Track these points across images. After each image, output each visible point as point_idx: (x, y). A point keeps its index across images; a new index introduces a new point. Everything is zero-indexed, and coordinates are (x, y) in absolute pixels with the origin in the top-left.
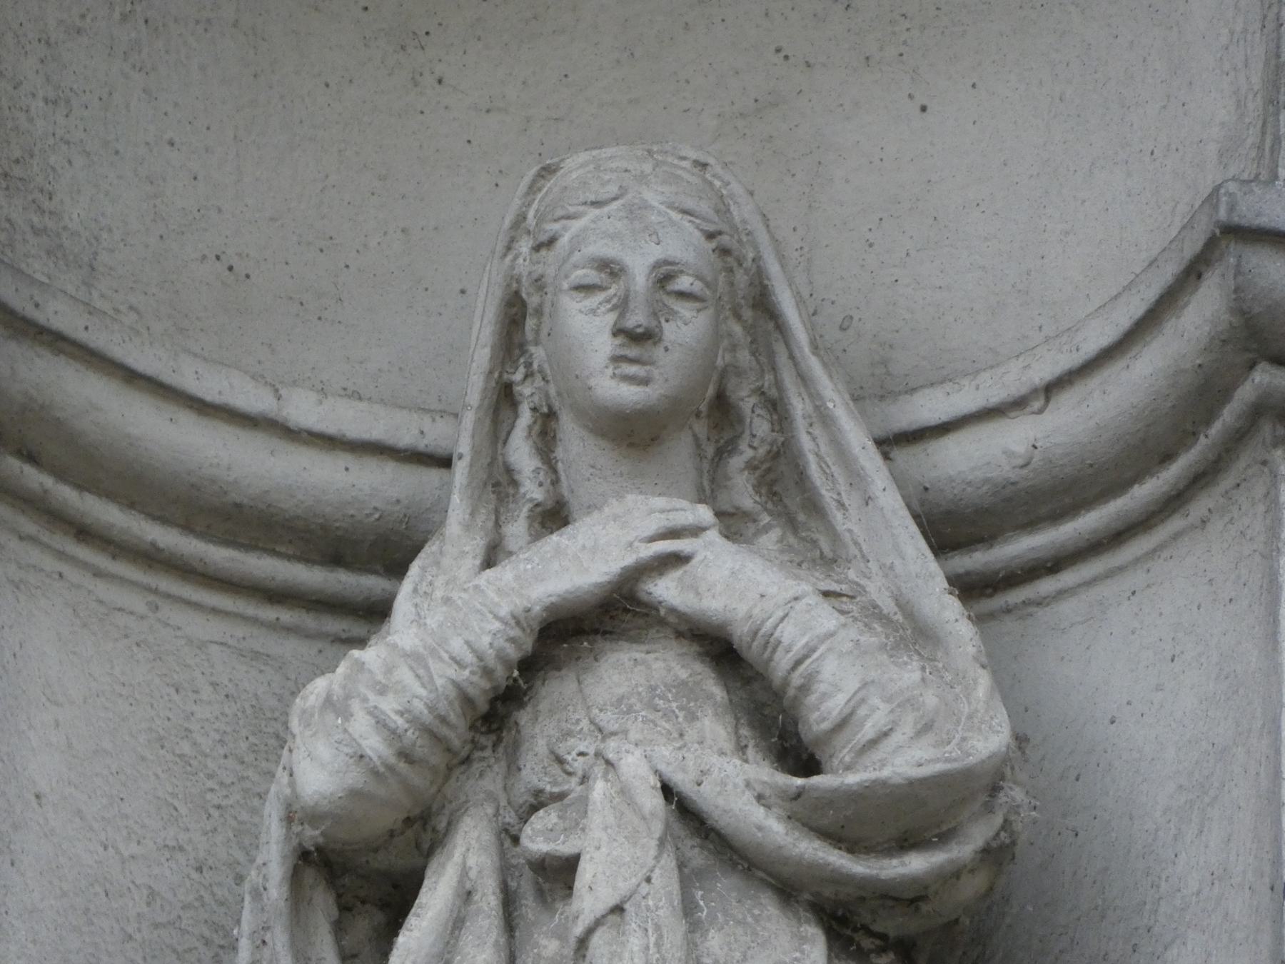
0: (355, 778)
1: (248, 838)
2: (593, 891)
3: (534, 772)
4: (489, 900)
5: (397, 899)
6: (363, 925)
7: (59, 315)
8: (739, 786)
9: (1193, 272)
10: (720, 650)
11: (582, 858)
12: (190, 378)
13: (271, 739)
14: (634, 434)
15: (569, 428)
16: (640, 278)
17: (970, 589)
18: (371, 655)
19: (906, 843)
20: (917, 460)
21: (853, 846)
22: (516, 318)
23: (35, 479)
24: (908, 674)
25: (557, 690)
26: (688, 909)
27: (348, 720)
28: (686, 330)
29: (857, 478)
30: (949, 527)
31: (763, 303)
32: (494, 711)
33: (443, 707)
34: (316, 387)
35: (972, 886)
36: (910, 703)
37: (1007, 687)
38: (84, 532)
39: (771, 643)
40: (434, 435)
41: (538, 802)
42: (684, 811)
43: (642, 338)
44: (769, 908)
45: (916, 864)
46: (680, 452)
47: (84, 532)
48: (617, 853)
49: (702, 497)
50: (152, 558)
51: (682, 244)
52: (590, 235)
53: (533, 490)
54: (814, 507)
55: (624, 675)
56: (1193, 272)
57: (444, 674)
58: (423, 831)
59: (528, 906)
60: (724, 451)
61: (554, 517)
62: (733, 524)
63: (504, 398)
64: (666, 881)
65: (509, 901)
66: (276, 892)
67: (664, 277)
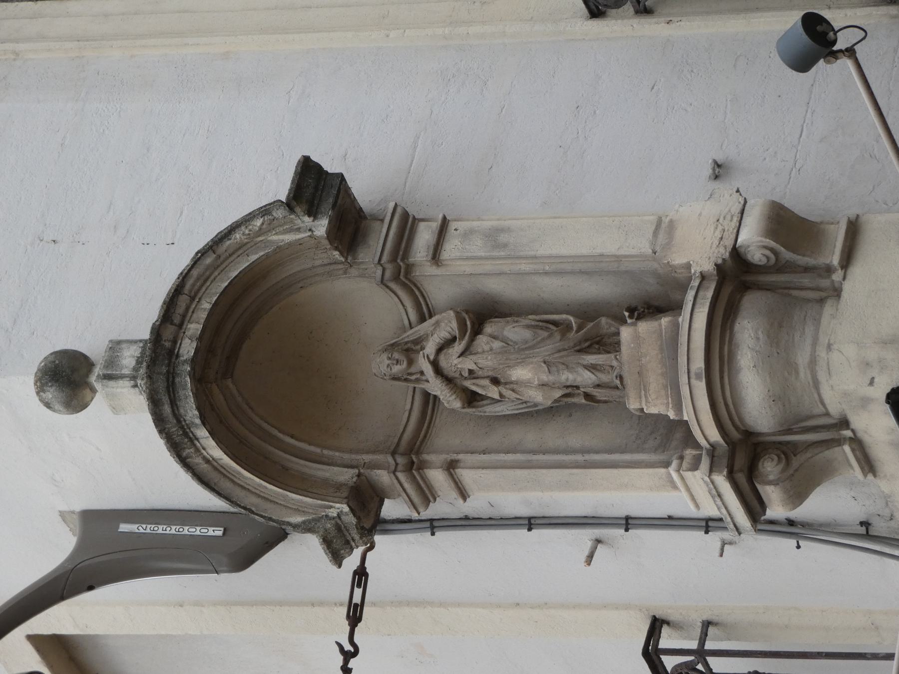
0: (458, 400)
1: (467, 413)
2: (473, 367)
3: (457, 375)
4: (474, 381)
5: (474, 394)
6: (478, 398)
7: (396, 440)
8: (458, 347)
9: (388, 287)
10: (440, 350)
11: (30, 633)
12: (404, 422)
13: (453, 411)
14: (411, 362)
15: (409, 371)
16: (389, 362)
17: (431, 316)
18: (441, 398)
19: (466, 325)
20: (413, 324)
21: (466, 332)
22: (395, 378)
23: (418, 443)
24: (443, 324)
25: (445, 372)
26: (475, 354)
27: (450, 400)
28: (396, 355)
29: (416, 332)
30: (422, 319)
31: (392, 345)
32: (449, 380)
33: (794, 458)
34: (403, 405)
35: (471, 315)
36: (446, 324)
37: (445, 311)
38: (425, 436)
39: (439, 343)
40: (411, 390)
41: (461, 374)
42: (462, 355)
43: (397, 361)
44: (475, 343)
45: (468, 323)
46: (413, 356)
47: (425, 436)
48: (468, 364)
49: (419, 353)
50: (429, 427)
51: (385, 356)
52: (384, 369)
53: (418, 376)
54: (420, 337)
55: (443, 363)
56: (388, 287)
57: (444, 388)
58: (465, 390)
59: (475, 375)
60: (412, 350)
61: (422, 373)
62: (423, 348)
63: (406, 380)
64: (471, 357)
65: (474, 378)
66: (474, 410)
67: (389, 359)
